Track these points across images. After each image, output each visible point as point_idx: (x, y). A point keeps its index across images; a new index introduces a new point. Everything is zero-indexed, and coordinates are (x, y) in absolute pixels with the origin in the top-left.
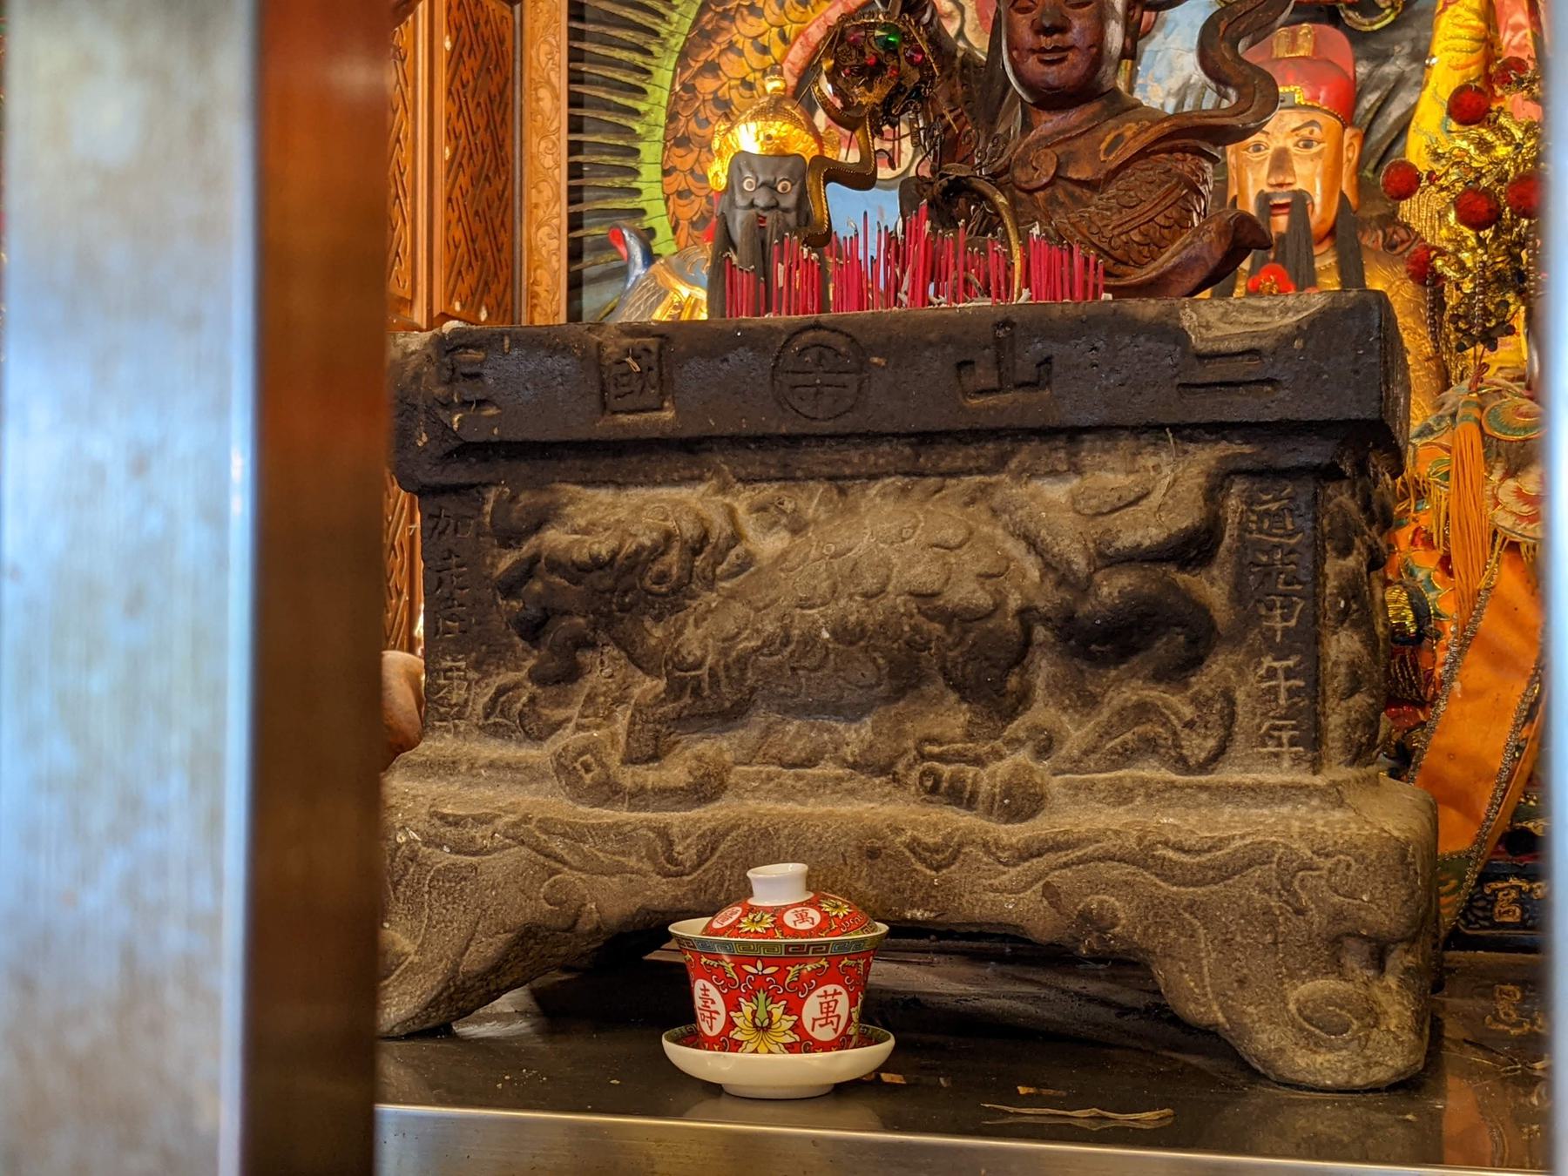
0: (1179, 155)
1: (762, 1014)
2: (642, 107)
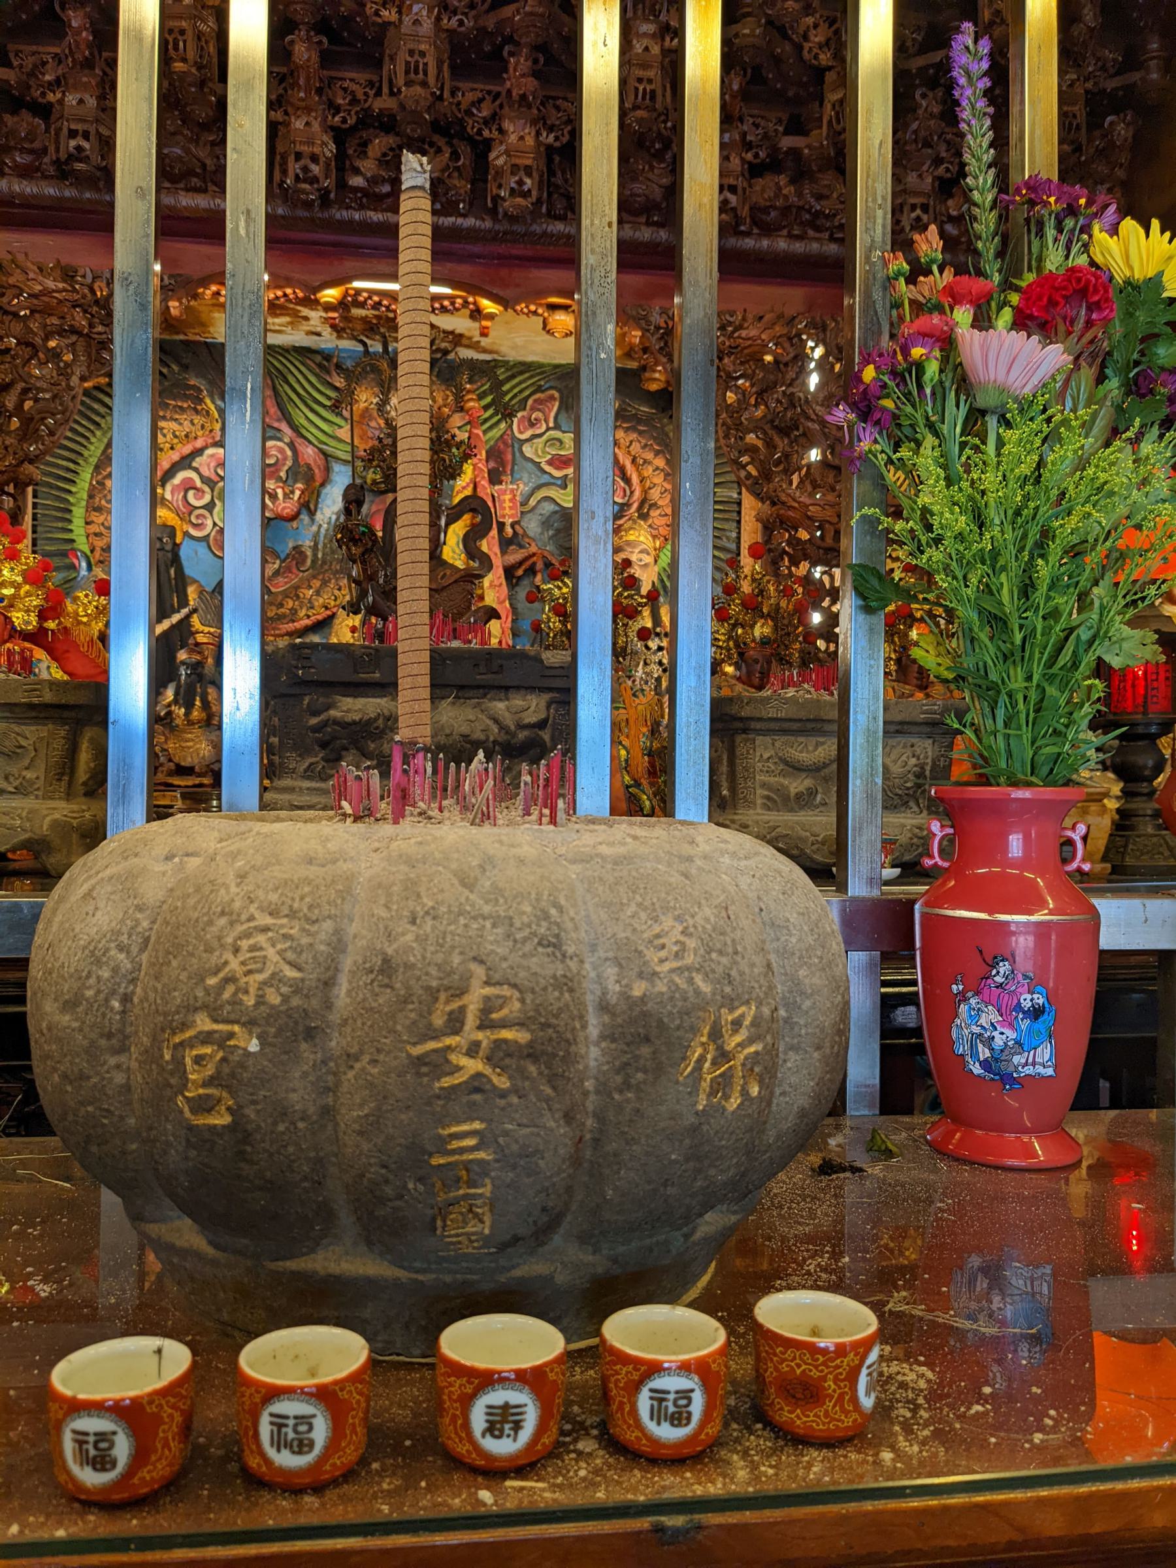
2: (73, 489)
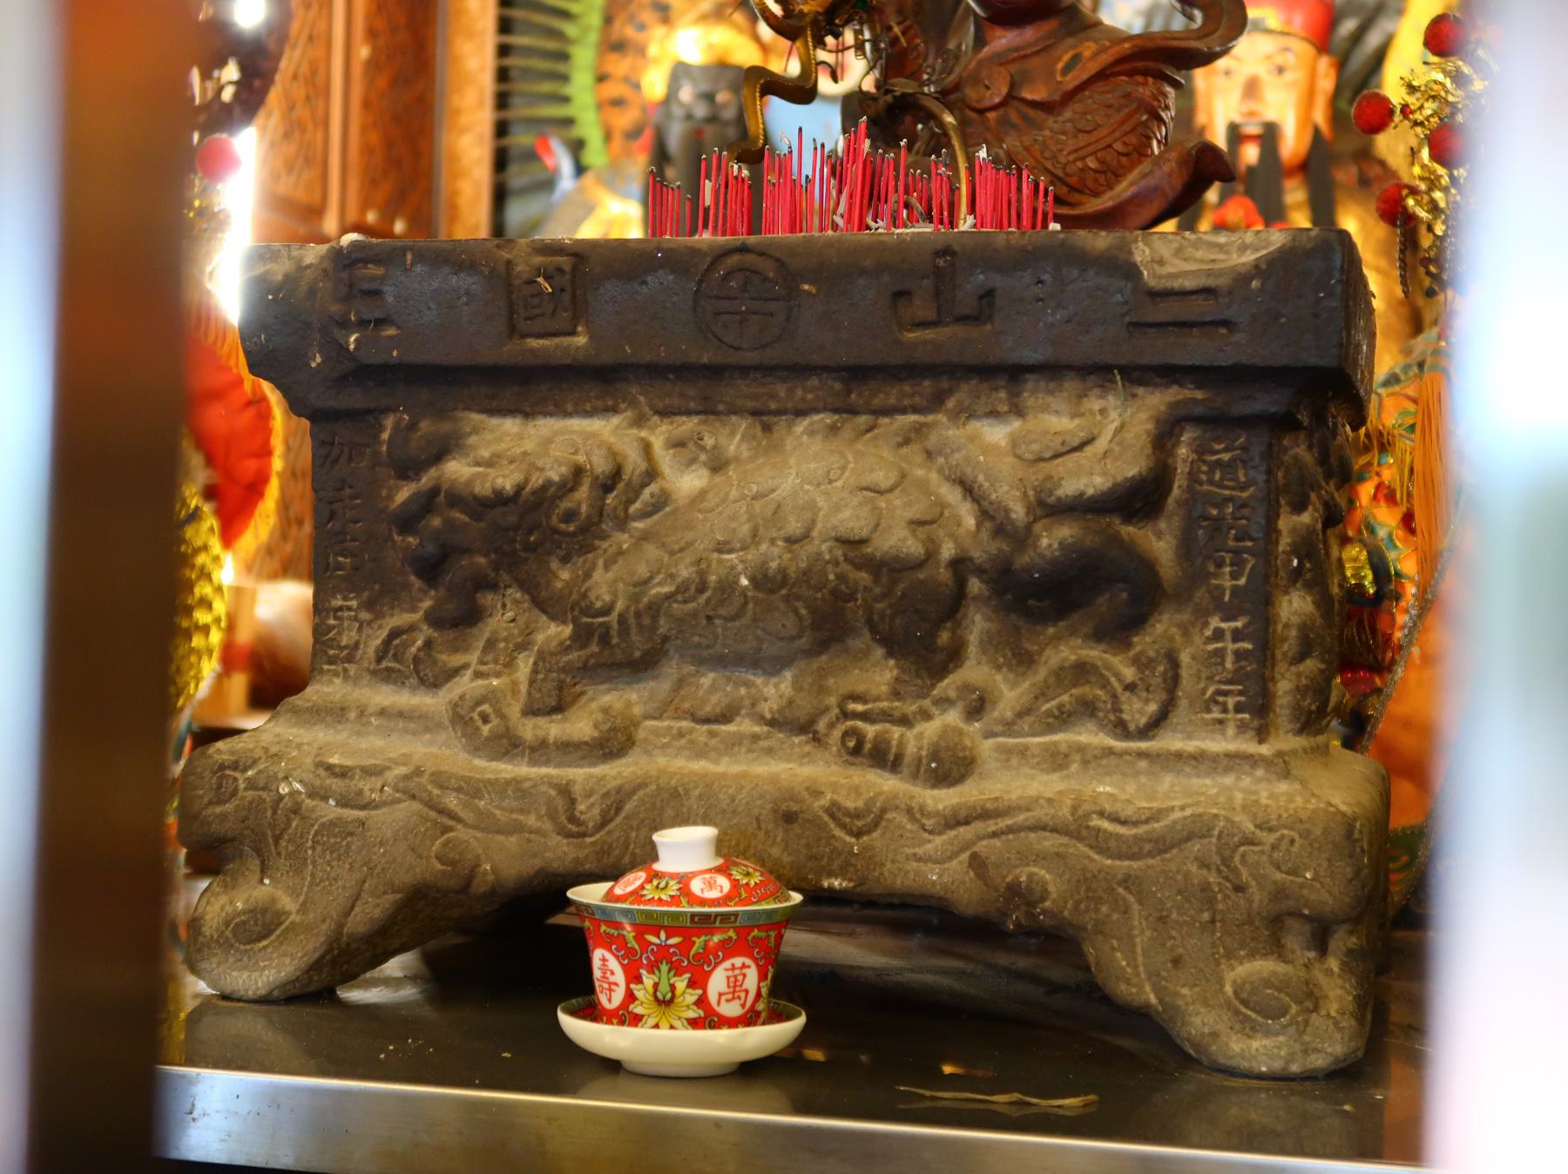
0: (1140, 79)
1: (664, 988)
